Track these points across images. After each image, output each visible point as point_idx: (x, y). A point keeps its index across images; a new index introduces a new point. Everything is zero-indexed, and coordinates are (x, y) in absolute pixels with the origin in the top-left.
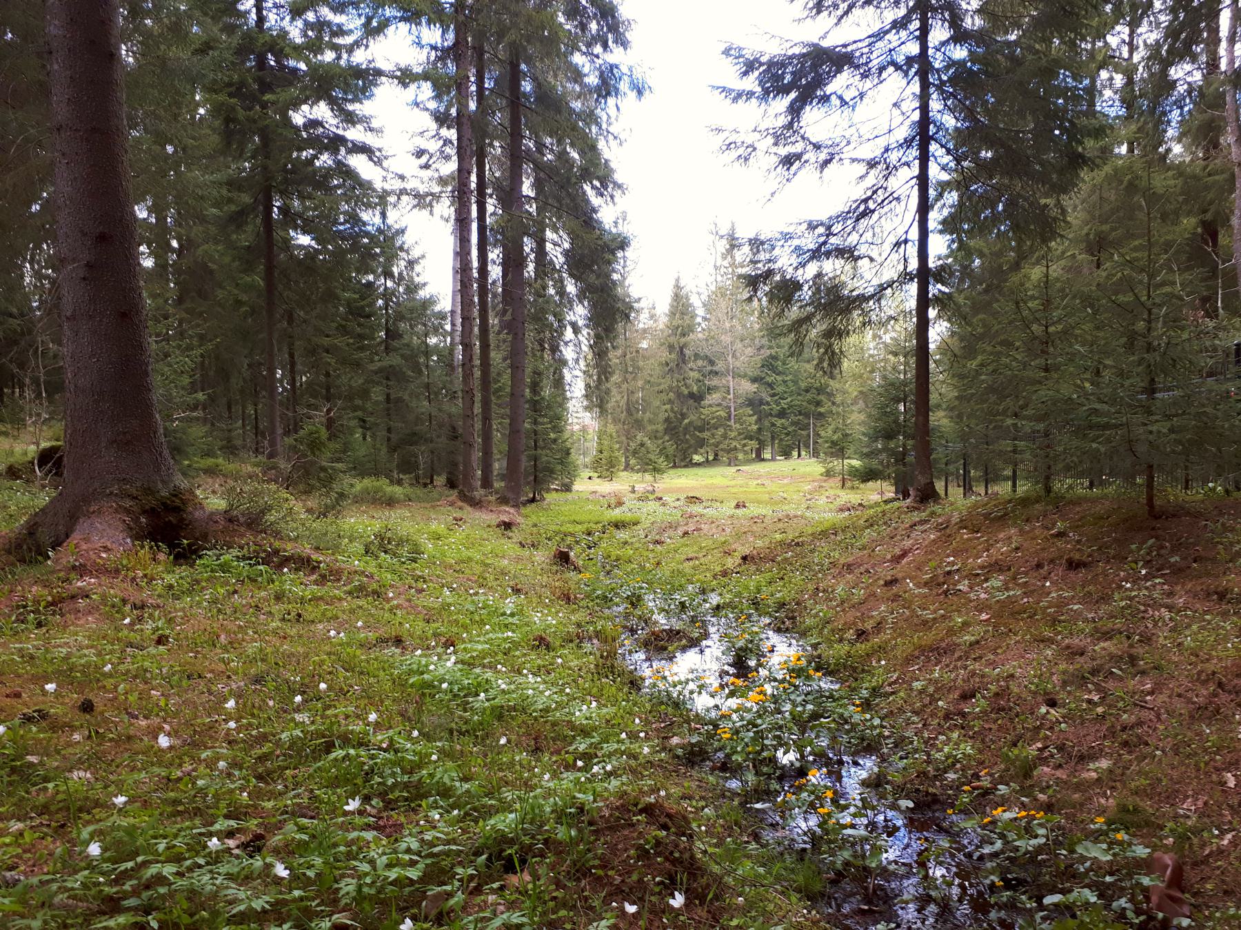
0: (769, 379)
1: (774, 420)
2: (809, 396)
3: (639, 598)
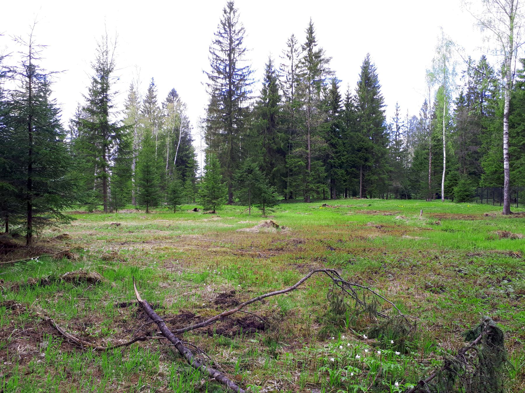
0: (334, 141)
1: (336, 170)
2: (360, 154)
3: (13, 310)
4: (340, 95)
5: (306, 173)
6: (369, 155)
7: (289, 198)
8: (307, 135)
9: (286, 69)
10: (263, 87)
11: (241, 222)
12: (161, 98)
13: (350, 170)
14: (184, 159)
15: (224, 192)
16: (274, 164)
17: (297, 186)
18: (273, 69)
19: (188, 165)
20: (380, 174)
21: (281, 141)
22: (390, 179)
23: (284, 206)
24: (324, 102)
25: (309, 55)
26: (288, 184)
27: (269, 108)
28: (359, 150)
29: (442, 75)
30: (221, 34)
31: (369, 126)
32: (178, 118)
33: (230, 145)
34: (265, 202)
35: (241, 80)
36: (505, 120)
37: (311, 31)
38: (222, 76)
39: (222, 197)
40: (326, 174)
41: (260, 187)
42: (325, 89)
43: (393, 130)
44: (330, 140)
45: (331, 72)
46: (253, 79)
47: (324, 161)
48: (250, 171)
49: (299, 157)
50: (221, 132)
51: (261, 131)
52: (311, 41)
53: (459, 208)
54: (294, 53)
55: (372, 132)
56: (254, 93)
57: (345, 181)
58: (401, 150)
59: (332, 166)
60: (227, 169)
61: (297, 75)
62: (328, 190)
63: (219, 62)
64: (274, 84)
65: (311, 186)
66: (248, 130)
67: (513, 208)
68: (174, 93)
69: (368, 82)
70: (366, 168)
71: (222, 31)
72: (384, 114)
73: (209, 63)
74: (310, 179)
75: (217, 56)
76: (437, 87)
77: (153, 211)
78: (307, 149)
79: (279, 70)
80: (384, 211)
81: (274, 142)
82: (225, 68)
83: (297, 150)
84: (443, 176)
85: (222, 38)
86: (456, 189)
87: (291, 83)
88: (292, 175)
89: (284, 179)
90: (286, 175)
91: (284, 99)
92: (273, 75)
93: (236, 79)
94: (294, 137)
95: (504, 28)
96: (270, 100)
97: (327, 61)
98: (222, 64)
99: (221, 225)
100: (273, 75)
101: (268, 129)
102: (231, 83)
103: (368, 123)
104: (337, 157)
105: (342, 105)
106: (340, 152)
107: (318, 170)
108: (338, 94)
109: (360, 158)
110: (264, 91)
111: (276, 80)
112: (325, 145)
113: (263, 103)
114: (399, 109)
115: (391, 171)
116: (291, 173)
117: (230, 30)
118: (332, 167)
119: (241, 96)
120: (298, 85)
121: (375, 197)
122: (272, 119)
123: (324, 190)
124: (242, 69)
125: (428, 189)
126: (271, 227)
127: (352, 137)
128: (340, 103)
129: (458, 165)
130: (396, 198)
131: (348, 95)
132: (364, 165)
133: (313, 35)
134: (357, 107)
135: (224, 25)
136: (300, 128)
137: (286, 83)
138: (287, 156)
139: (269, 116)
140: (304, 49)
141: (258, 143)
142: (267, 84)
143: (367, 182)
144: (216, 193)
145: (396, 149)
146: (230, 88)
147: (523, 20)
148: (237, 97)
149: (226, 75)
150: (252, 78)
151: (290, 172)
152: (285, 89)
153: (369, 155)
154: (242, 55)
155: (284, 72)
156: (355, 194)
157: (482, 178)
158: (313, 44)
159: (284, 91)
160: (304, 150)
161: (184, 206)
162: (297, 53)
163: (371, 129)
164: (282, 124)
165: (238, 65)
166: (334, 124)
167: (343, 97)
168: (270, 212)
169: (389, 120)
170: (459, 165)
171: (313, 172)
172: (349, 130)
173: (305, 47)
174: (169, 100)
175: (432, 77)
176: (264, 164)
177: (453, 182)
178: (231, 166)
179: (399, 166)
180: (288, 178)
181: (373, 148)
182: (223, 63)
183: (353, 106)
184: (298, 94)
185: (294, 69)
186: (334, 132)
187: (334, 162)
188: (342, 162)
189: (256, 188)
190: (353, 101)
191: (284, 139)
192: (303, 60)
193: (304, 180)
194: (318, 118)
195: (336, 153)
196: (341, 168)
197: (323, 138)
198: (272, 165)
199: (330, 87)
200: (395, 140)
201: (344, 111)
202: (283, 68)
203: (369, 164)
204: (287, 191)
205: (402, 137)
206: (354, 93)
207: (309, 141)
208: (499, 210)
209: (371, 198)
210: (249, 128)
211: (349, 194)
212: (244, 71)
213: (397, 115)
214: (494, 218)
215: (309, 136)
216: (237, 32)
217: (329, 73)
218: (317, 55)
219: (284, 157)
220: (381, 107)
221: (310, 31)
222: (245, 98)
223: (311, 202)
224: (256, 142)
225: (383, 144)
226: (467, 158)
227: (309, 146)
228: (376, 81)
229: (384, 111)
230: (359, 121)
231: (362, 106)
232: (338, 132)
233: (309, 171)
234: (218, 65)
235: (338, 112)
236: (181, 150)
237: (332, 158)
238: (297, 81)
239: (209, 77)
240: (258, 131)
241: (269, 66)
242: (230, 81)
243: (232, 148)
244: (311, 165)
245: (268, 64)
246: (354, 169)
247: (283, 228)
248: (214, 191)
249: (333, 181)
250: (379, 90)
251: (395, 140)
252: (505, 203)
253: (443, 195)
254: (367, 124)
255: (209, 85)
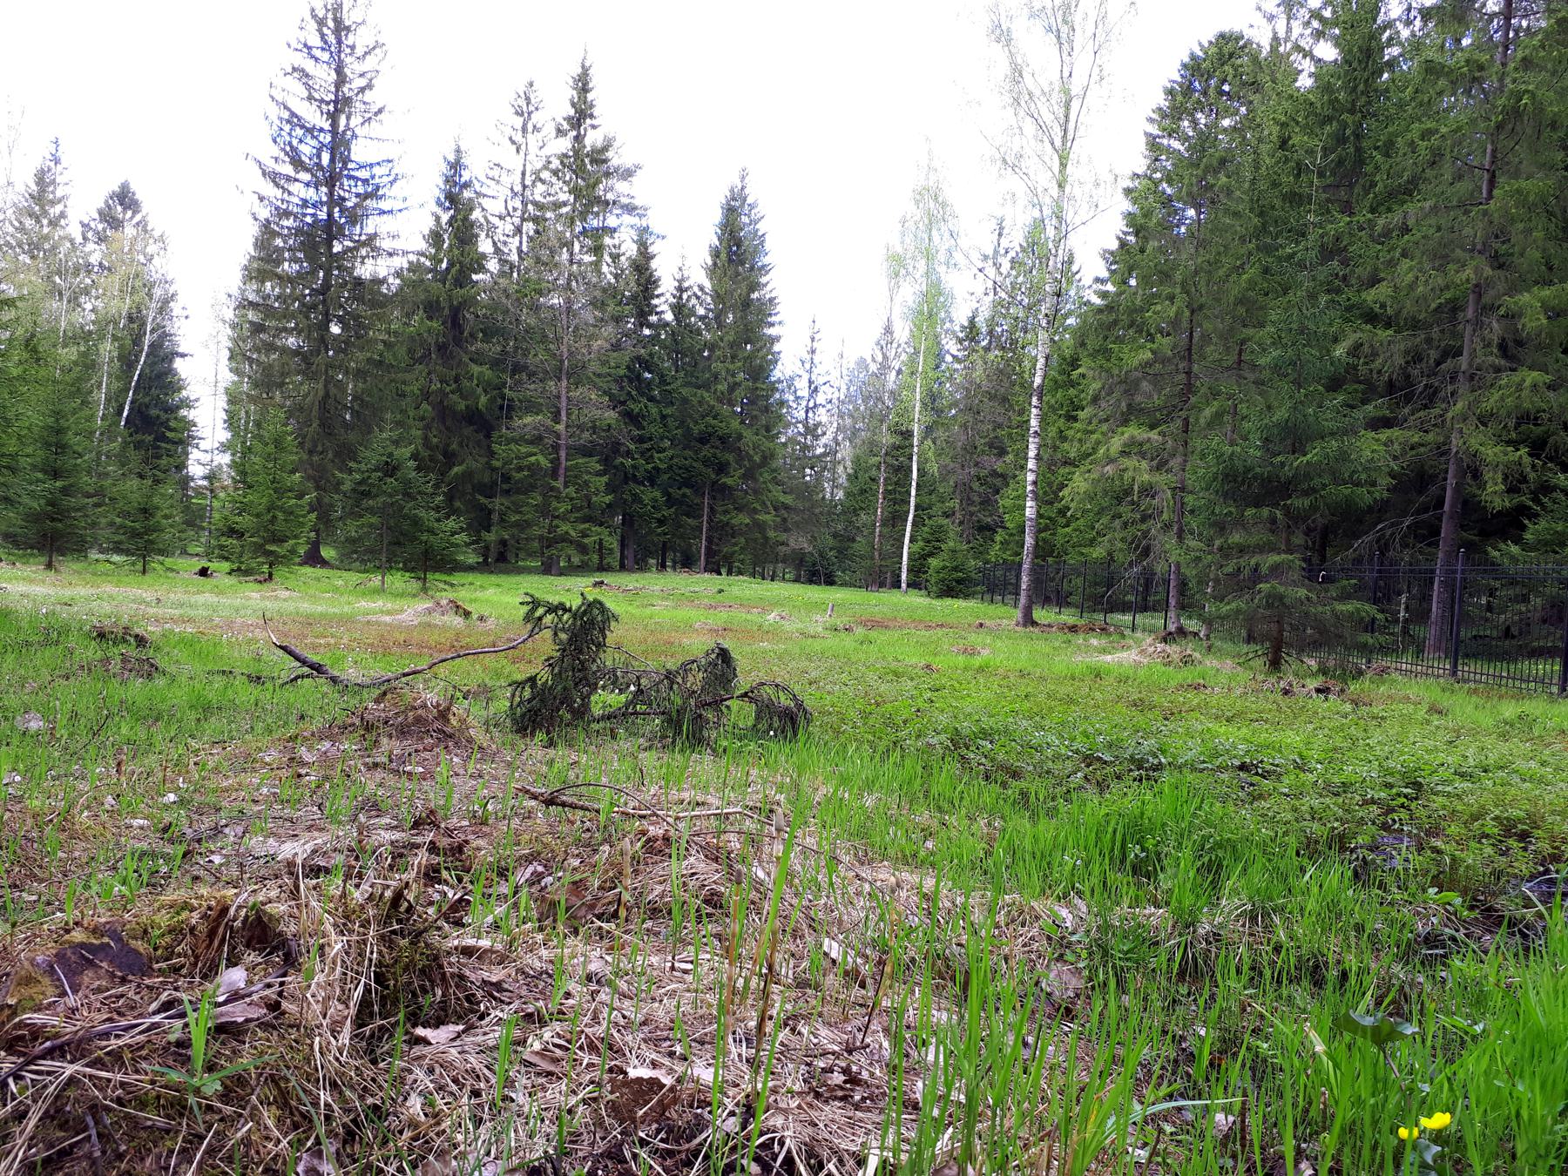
1: (638, 489)
2: (706, 451)
4: (659, 279)
5: (552, 489)
6: (730, 457)
7: (497, 560)
8: (560, 379)
9: (506, 180)
10: (431, 223)
11: (360, 614)
12: (81, 204)
13: (676, 493)
14: (154, 412)
15: (302, 525)
16: (454, 454)
17: (523, 525)
18: (466, 176)
19: (169, 434)
20: (755, 511)
21: (480, 390)
22: (784, 526)
23: (478, 579)
24: (612, 292)
25: (576, 152)
26: (495, 517)
27: (449, 286)
28: (703, 440)
29: (922, 265)
30: (309, 48)
31: (733, 376)
32: (140, 284)
33: (321, 386)
34: (430, 564)
35: (367, 196)
36: (1034, 401)
37: (585, 84)
38: (305, 177)
39: (296, 537)
40: (608, 499)
41: (416, 515)
42: (615, 258)
43: (799, 393)
44: (623, 403)
45: (635, 208)
46: (405, 199)
47: (606, 461)
48: (390, 469)
49: (531, 442)
50: (291, 341)
51: (419, 353)
52: (582, 114)
53: (931, 608)
54: (529, 136)
55: (739, 393)
56: (400, 237)
57: (661, 522)
58: (819, 451)
59: (629, 477)
60: (305, 457)
61: (535, 204)
62: (613, 543)
63: (299, 132)
64: (466, 219)
65: (565, 527)
66: (381, 347)
67: (1039, 614)
68: (125, 198)
69: (737, 253)
70: (721, 491)
71: (315, 41)
72: (776, 348)
73: (265, 133)
74: (563, 508)
75: (293, 114)
76: (909, 293)
77: (69, 566)
78: (557, 420)
79: (483, 179)
80: (746, 605)
81: (459, 390)
82: (319, 156)
83: (528, 421)
84: (909, 528)
85: (312, 62)
86: (934, 562)
87: (517, 221)
88: (507, 492)
89: (483, 500)
90: (489, 490)
91: (493, 265)
92: (467, 194)
93: (349, 192)
94: (520, 382)
95: (1045, 179)
96: (451, 264)
97: (627, 174)
98: (308, 139)
99: (306, 607)
100: (467, 194)
101: (441, 348)
102: (334, 201)
103: (731, 367)
104: (642, 454)
105: (663, 305)
106: (650, 439)
107: (586, 483)
108: (651, 275)
109: (706, 462)
110: (435, 237)
111: (472, 210)
112: (611, 416)
113: (431, 271)
114: (817, 337)
115: (786, 507)
116: (505, 487)
117: (339, 42)
118: (626, 480)
119: (364, 244)
120: (537, 232)
121: (740, 573)
122: (455, 320)
123: (601, 544)
124: (371, 165)
125: (872, 558)
126: (452, 613)
127: (685, 401)
128: (655, 302)
129: (951, 504)
130: (797, 580)
131: (680, 281)
132: (714, 483)
133: (590, 96)
134: (702, 318)
135: (321, 23)
136: (538, 357)
137: (501, 218)
138: (495, 434)
139: (446, 312)
140: (560, 132)
141: (408, 389)
142: (445, 217)
143: (721, 531)
144: (280, 526)
145: (805, 447)
146: (330, 215)
147: (1393, 8)
148: (350, 244)
149: (320, 174)
150: (400, 197)
151: (503, 483)
152: (499, 237)
153: (730, 457)
154: (373, 123)
155: (499, 188)
156: (687, 563)
157: (998, 538)
158: (588, 121)
159: (494, 243)
160: (549, 423)
161: (181, 563)
162: (539, 136)
163: (738, 384)
164: (486, 340)
165: (360, 152)
166: (638, 358)
167: (667, 287)
168: (442, 586)
169: (788, 363)
170: (955, 504)
171: (571, 490)
172: (679, 382)
173: (566, 126)
174: (108, 217)
175: (897, 266)
176: (425, 453)
177: (931, 545)
178: (320, 448)
179: (808, 492)
180: (497, 501)
181: (740, 437)
182: (313, 137)
183: (694, 314)
184: (538, 261)
185: (528, 182)
186: (636, 382)
187: (634, 467)
188: (657, 469)
189: (406, 517)
190: (694, 301)
191: (489, 383)
192: (556, 164)
193: (544, 510)
194: (593, 337)
195: (641, 440)
196: (652, 486)
197: (605, 392)
198: (450, 458)
199: (630, 249)
200: (805, 422)
201: (667, 324)
202: (495, 173)
203: (729, 481)
204: (491, 537)
205: (822, 416)
206: (699, 277)
207: (564, 399)
208: (1006, 615)
209: (729, 573)
210: (384, 342)
211: (675, 562)
212: (377, 170)
213: (813, 352)
214: (996, 632)
215: (564, 383)
216: (359, 51)
217: (630, 209)
218: (599, 156)
219: (488, 436)
220: (772, 325)
221: (583, 84)
222: (376, 252)
223: (561, 574)
224: (404, 383)
225: (768, 430)
226: (976, 485)
227: (563, 413)
228: (759, 249)
229: (778, 339)
230: (709, 358)
231: (719, 317)
232: (649, 383)
233: (559, 484)
234: (295, 142)
235: (650, 326)
236: (144, 385)
237: (628, 453)
238: (535, 220)
239: (264, 174)
240: (411, 351)
241: (456, 166)
242: (331, 194)
243: (327, 395)
244: (567, 469)
245: (452, 158)
246: (688, 491)
247: (481, 619)
248: (274, 517)
249: (628, 521)
250: (763, 280)
251: (805, 422)
252: (1023, 600)
253: (904, 576)
254: (728, 370)
255: (261, 199)
